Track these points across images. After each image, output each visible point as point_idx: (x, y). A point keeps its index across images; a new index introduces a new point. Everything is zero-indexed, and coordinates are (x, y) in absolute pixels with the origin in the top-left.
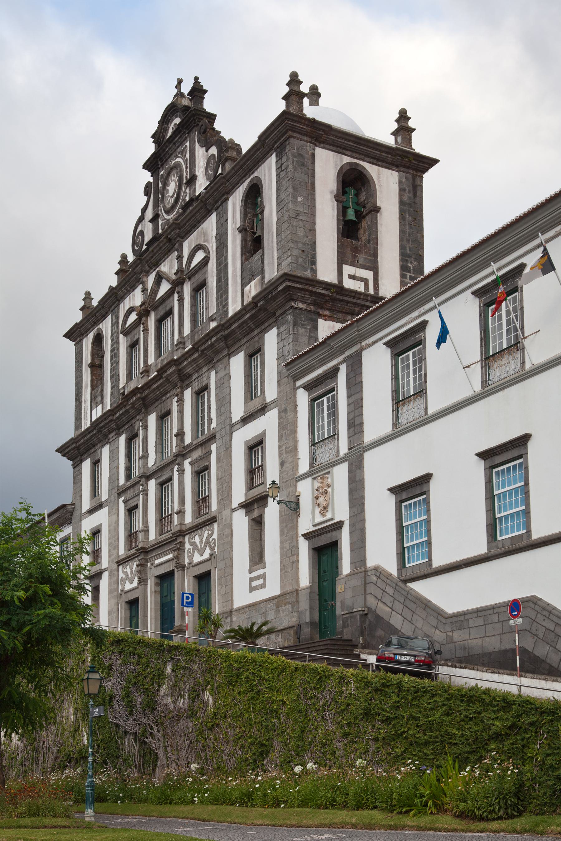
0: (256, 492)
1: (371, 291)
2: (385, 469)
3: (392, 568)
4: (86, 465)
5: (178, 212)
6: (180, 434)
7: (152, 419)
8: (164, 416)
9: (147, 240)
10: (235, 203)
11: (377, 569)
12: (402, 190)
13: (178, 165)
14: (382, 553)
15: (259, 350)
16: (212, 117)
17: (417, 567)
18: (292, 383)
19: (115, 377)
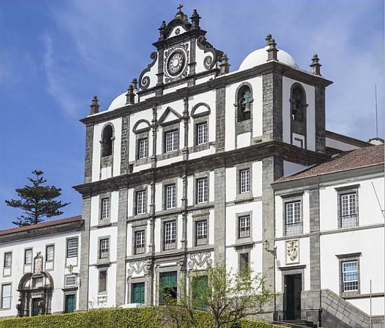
0: (103, 261)
1: (304, 147)
3: (337, 291)
5: (180, 77)
11: (327, 290)
14: (330, 281)
18: (273, 192)
19: (125, 154)
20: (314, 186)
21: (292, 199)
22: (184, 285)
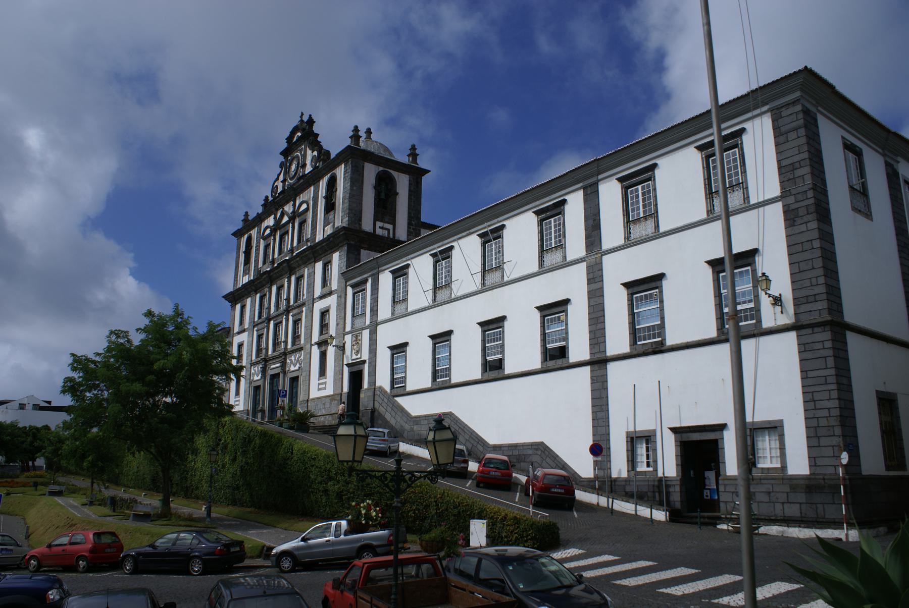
0: (324, 337)
2: (388, 335)
3: (387, 387)
4: (238, 307)
6: (288, 300)
7: (274, 288)
8: (279, 289)
9: (279, 191)
10: (323, 184)
11: (380, 387)
12: (410, 184)
13: (297, 156)
14: (383, 380)
15: (330, 262)
16: (317, 135)
17: (398, 386)
19: (257, 261)
20: (376, 271)
21: (359, 287)
22: (284, 384)
